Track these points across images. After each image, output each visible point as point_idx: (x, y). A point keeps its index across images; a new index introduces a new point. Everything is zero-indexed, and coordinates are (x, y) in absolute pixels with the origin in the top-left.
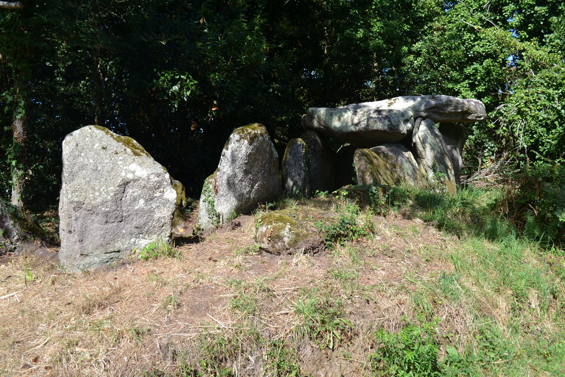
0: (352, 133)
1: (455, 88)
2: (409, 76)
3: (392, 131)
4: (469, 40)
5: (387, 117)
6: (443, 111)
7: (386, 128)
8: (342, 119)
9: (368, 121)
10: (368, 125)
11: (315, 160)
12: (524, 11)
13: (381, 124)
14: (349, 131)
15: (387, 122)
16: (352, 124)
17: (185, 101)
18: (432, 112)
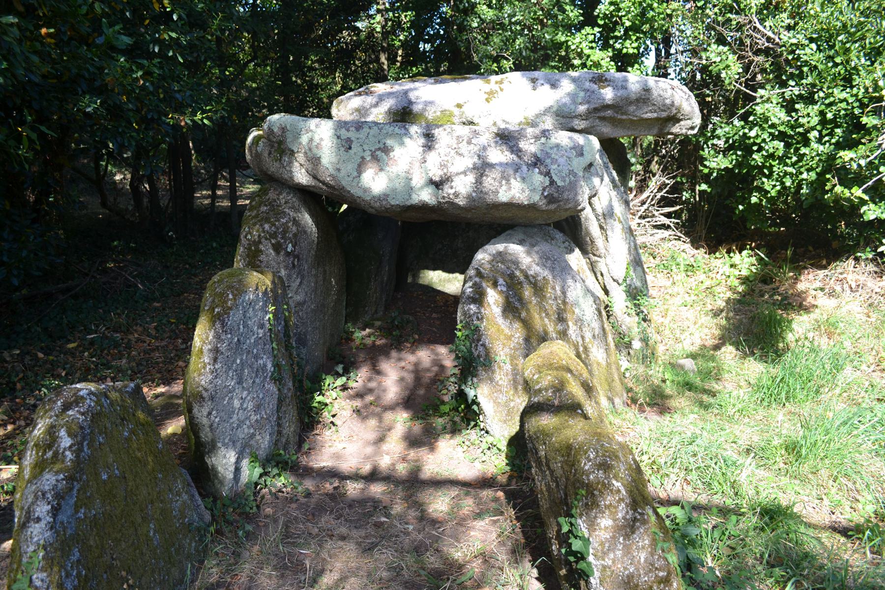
1: (570, 43)
2: (476, 13)
3: (552, 207)
5: (537, 162)
6: (624, 117)
11: (299, 280)
15: (538, 179)
18: (599, 117)
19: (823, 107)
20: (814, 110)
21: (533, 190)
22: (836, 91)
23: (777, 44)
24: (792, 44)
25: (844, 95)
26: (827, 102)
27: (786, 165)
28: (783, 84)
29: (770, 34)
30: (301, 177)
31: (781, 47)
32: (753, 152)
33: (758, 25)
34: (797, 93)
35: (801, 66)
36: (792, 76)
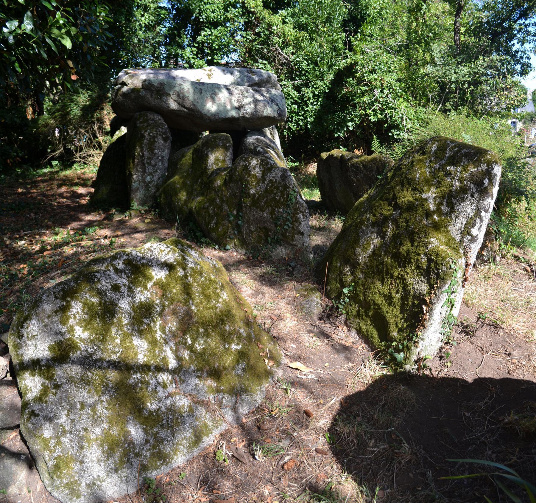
0: (232, 120)
7: (276, 114)
9: (256, 105)
14: (228, 116)
20: (309, 90)
21: (274, 111)
23: (289, 61)
24: (297, 61)
26: (315, 86)
27: (300, 116)
28: (293, 79)
30: (173, 105)
31: (292, 62)
33: (280, 51)
36: (297, 75)
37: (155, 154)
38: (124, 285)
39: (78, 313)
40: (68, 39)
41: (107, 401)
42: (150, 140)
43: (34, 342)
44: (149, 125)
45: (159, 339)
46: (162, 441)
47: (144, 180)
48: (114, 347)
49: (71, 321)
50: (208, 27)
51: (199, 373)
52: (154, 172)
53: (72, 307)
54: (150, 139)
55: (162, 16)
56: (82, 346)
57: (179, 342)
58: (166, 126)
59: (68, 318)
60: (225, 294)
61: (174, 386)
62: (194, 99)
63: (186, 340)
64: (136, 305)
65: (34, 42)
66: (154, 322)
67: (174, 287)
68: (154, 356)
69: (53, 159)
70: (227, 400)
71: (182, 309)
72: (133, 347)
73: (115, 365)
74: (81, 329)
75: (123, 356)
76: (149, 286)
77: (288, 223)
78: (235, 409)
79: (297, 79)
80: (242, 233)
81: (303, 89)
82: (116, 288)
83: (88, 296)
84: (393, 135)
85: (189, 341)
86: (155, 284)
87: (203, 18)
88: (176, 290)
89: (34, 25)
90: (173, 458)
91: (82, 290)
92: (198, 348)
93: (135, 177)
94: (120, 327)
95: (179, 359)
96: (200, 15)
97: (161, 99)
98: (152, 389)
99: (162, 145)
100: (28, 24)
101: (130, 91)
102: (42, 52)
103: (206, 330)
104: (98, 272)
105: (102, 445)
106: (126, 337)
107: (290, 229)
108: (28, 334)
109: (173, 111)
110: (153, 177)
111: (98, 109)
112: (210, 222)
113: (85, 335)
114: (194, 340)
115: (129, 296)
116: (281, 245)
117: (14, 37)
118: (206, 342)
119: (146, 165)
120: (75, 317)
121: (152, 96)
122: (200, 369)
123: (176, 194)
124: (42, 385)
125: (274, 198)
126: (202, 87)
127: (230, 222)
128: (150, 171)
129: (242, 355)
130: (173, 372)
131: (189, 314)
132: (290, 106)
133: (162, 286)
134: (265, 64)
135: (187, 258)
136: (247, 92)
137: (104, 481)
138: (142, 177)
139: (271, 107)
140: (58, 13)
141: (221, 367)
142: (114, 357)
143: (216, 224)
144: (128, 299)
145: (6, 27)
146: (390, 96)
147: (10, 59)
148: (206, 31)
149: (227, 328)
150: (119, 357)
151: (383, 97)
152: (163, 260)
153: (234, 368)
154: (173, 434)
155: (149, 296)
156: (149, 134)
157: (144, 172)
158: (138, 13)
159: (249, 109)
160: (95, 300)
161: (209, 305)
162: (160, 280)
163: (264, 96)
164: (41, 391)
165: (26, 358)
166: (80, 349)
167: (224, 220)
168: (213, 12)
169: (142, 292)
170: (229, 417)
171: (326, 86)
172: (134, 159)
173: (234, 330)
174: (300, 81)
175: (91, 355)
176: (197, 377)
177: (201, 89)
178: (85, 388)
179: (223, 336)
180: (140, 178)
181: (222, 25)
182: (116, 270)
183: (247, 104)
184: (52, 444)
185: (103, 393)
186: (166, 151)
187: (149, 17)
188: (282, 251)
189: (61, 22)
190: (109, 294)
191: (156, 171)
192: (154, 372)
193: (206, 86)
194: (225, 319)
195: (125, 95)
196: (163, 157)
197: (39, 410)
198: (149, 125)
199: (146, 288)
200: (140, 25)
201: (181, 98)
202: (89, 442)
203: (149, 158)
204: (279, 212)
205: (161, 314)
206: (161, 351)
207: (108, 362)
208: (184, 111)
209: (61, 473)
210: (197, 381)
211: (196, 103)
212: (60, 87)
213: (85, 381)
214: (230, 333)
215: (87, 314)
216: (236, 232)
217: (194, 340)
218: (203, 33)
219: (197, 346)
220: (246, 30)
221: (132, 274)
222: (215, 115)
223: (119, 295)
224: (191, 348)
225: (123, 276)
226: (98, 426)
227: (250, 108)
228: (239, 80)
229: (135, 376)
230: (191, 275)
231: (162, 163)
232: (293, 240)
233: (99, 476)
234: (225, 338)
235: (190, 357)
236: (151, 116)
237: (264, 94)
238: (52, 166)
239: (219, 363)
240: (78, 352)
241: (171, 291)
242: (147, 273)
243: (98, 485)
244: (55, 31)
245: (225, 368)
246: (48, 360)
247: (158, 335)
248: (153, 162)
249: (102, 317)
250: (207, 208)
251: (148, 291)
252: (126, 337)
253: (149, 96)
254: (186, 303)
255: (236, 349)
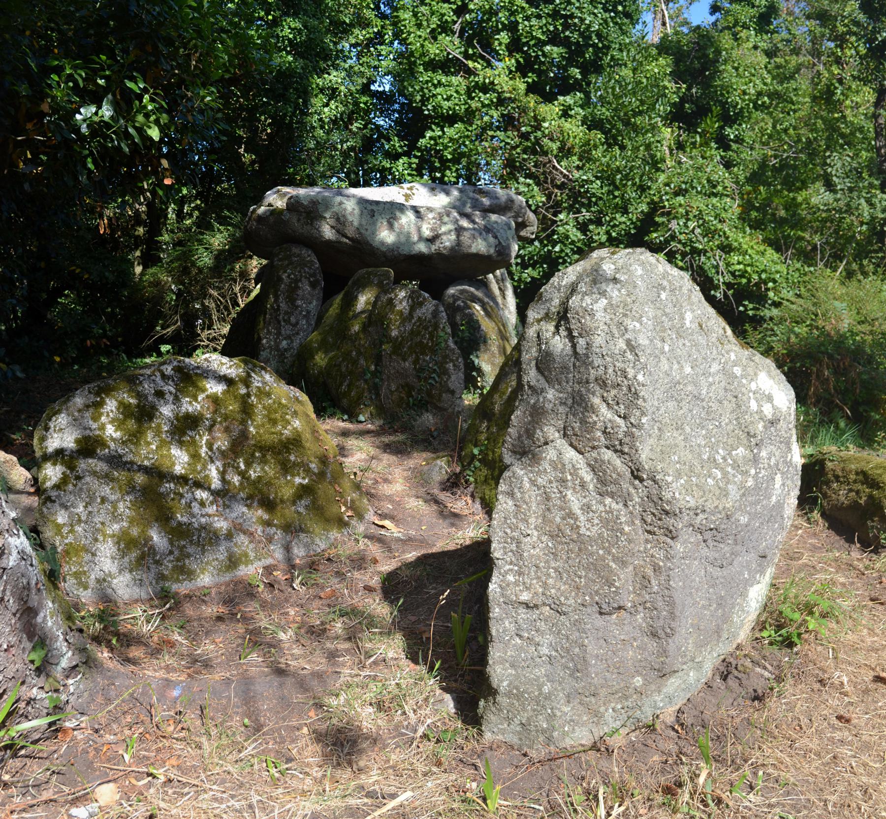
0: (420, 258)
4: (430, 84)
7: (492, 251)
8: (396, 225)
9: (458, 236)
10: (459, 243)
12: (526, 49)
13: (484, 243)
14: (414, 252)
16: (421, 238)
17: (124, 153)
19: (609, 228)
21: (490, 246)
22: (618, 216)
23: (571, 180)
24: (583, 180)
25: (623, 219)
26: (612, 224)
29: (565, 171)
30: (328, 232)
31: (574, 182)
32: (559, 264)
33: (556, 164)
34: (588, 217)
35: (590, 197)
36: (583, 205)
37: (297, 307)
38: (171, 393)
39: (112, 411)
40: (156, 128)
41: (131, 501)
42: (290, 286)
43: (60, 435)
44: (291, 263)
45: (203, 455)
46: (188, 556)
47: (278, 346)
48: (148, 453)
49: (103, 419)
50: (437, 125)
51: (249, 501)
52: (293, 335)
53: (106, 404)
54: (291, 283)
55: (362, 105)
56: (112, 445)
57: (229, 463)
58: (317, 266)
59: (101, 415)
60: (297, 422)
61: (215, 507)
62: (360, 225)
63: (238, 463)
64: (181, 415)
65: (113, 132)
66: (200, 435)
67: (231, 405)
68: (194, 471)
69: (163, 340)
70: (279, 534)
71: (236, 428)
72: (170, 456)
73: (146, 470)
74: (113, 428)
75: (157, 464)
76: (200, 399)
77: (434, 375)
78: (287, 549)
79: (584, 210)
80: (380, 395)
81: (591, 227)
82: (160, 394)
83: (125, 396)
84: (746, 310)
85: (242, 466)
86: (208, 397)
87: (428, 110)
88: (233, 407)
89: (115, 111)
90: (198, 576)
91: (120, 389)
92: (253, 476)
93: (264, 341)
94: (158, 432)
95: (223, 480)
96: (423, 105)
97: (311, 224)
98: (186, 503)
99: (309, 292)
100: (108, 110)
101: (268, 213)
102: (123, 145)
103: (264, 456)
104: (142, 375)
105: (118, 543)
106: (163, 444)
107: (438, 385)
108: (55, 427)
109: (329, 242)
110: (292, 342)
111: (243, 257)
112: (341, 384)
113: (117, 435)
114: (248, 464)
115: (174, 404)
116: (427, 411)
117: (88, 126)
118: (262, 469)
119: (283, 324)
120: (108, 415)
121: (299, 220)
122: (250, 497)
123: (312, 357)
124: (63, 474)
125: (421, 342)
126: (374, 208)
127: (366, 381)
128: (288, 332)
129: (304, 491)
130: (216, 493)
131: (244, 435)
132: (569, 257)
133: (215, 400)
134: (529, 185)
135: (253, 375)
136: (448, 215)
137: (115, 578)
138: (275, 341)
139: (485, 240)
140: (147, 97)
141: (278, 500)
142: (146, 463)
143: (349, 385)
144: (172, 406)
145: (80, 114)
146: (698, 231)
147: (80, 153)
148: (433, 131)
149: (292, 458)
150: (153, 464)
151: (686, 234)
152: (222, 374)
153: (294, 503)
154: (203, 551)
155: (199, 408)
156: (289, 276)
157: (279, 334)
158: (317, 101)
159: (448, 241)
160: (133, 401)
161: (273, 430)
162: (216, 394)
163: (474, 222)
164: (61, 479)
165: (50, 450)
166: (109, 447)
167: (359, 380)
168: (448, 99)
169: (190, 403)
170: (279, 554)
171: (632, 223)
172: (265, 314)
173: (302, 462)
174: (588, 215)
175: (120, 456)
176: (247, 505)
177: (373, 211)
178: (108, 485)
179: (286, 466)
180: (272, 343)
181: (463, 122)
182: (164, 377)
183: (445, 233)
184: (65, 530)
185: (128, 493)
186: (314, 303)
187: (337, 107)
188: (429, 419)
189: (150, 108)
190: (150, 398)
191: (298, 334)
192: (191, 487)
193: (381, 207)
194: (291, 447)
195: (260, 219)
196: (308, 312)
197: (56, 496)
198: (291, 263)
199: (196, 400)
200: (321, 120)
201: (340, 221)
202: (104, 535)
203: (286, 313)
204: (424, 360)
205: (210, 429)
206: (204, 468)
207: (140, 466)
208: (346, 243)
209: (70, 559)
210: (245, 509)
211: (363, 231)
212: (148, 194)
213: (107, 478)
214: (295, 464)
215: (122, 413)
216: (373, 397)
217: (248, 464)
218: (429, 134)
219: (252, 473)
220: (505, 130)
221: (181, 382)
222: (395, 247)
223: (162, 401)
224: (243, 474)
225: (170, 382)
226: (116, 523)
227: (449, 240)
228: (457, 203)
229: (167, 485)
230: (256, 395)
231: (307, 321)
232: (439, 400)
233: (110, 572)
234: (286, 468)
235: (241, 484)
236: (295, 250)
237: (477, 220)
238: (160, 354)
239: (276, 493)
240: (107, 450)
241: (226, 408)
242: (200, 385)
243: (109, 582)
244: (140, 118)
245: (282, 501)
246: (72, 451)
247: (203, 451)
248: (293, 320)
249: (139, 421)
250: (339, 365)
251: (199, 403)
252: (163, 444)
253: (295, 220)
254: (243, 422)
255: (301, 484)
